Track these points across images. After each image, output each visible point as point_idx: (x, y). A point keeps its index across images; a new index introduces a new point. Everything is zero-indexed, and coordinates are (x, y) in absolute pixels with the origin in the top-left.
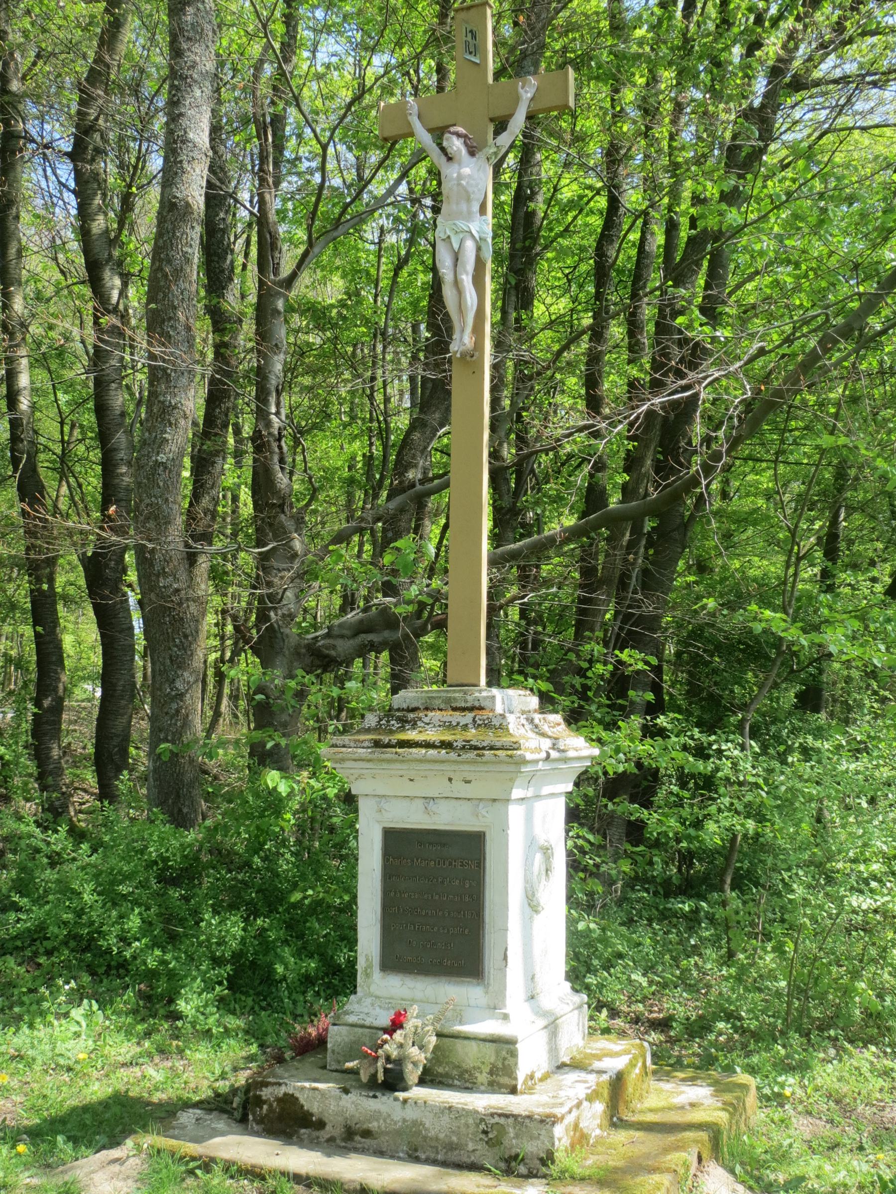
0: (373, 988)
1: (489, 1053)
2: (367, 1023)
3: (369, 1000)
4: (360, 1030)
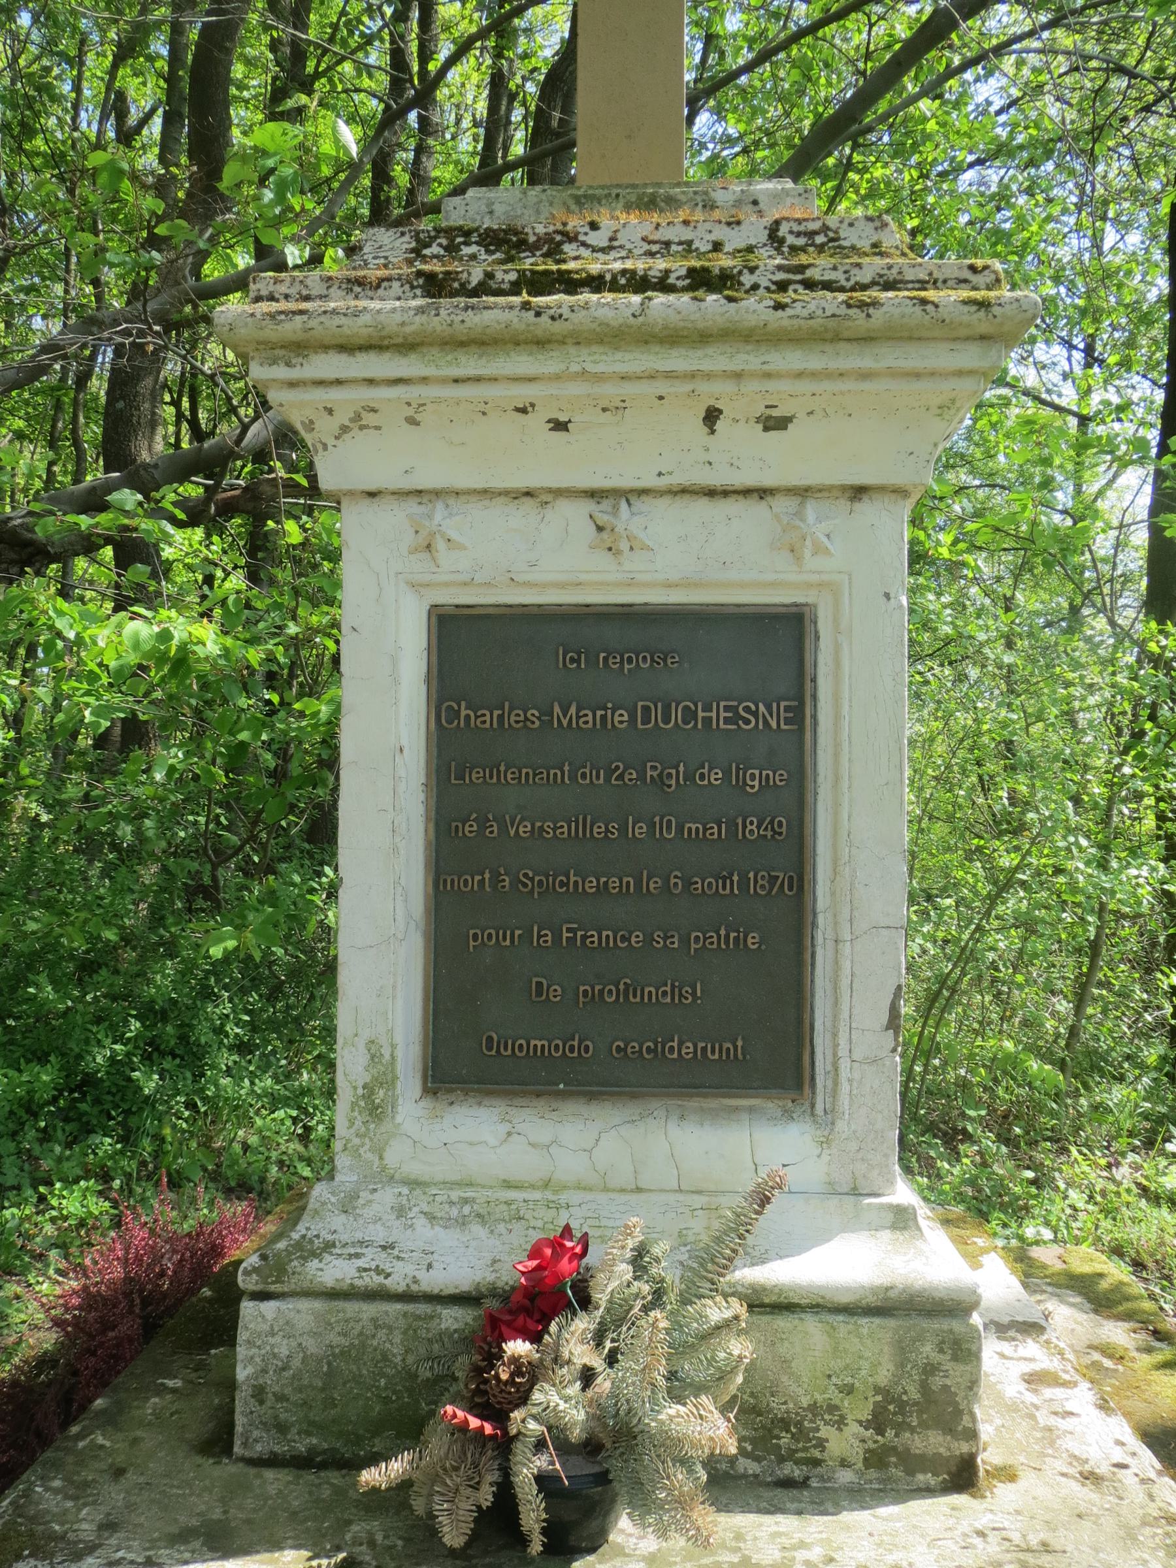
0: (397, 1155)
1: (872, 1354)
2: (397, 1283)
3: (387, 1197)
4: (369, 1310)
